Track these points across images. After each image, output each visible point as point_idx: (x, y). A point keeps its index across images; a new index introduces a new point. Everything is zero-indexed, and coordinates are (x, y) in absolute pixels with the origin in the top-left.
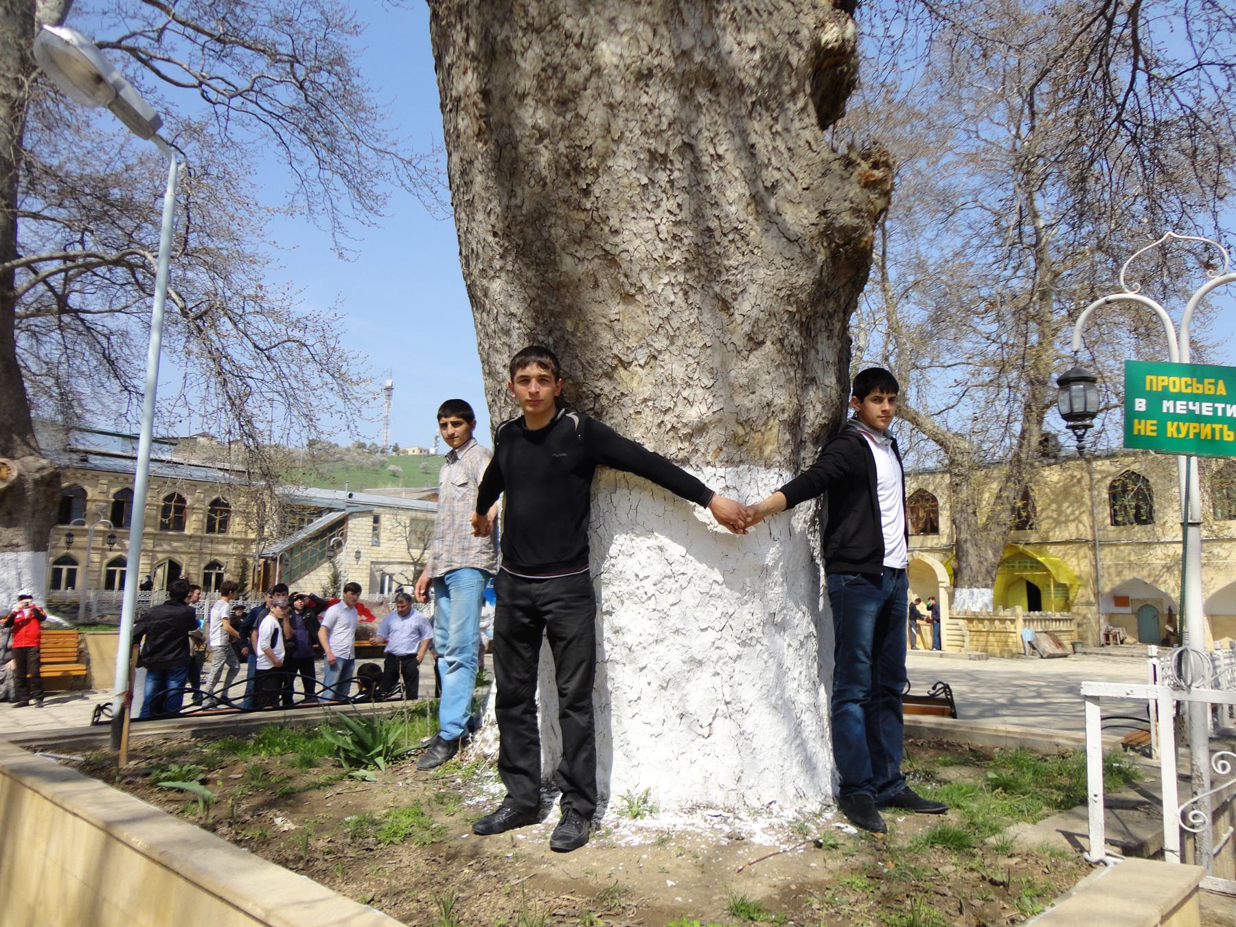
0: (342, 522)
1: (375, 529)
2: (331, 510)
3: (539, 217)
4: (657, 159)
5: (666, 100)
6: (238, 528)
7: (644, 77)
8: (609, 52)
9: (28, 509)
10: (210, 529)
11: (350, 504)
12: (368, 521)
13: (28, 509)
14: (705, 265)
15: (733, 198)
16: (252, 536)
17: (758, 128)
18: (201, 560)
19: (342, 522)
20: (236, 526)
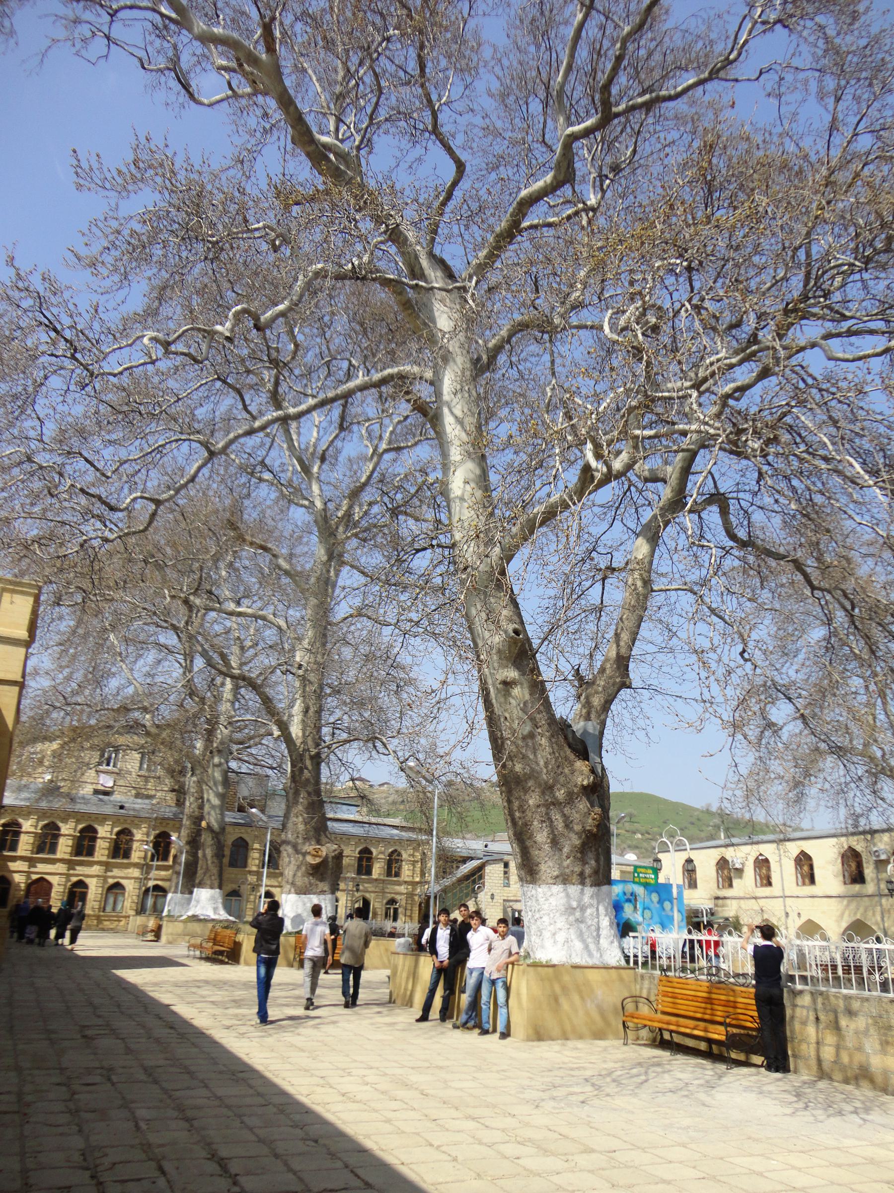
0: (481, 868)
1: (505, 873)
2: (472, 859)
3: (521, 833)
4: (543, 822)
5: (543, 809)
6: (407, 873)
7: (538, 806)
8: (531, 802)
9: (329, 872)
10: (389, 874)
11: (488, 854)
12: (500, 867)
13: (329, 872)
14: (555, 842)
15: (560, 825)
16: (418, 879)
17: (567, 810)
18: (383, 898)
19: (481, 868)
20: (406, 871)
